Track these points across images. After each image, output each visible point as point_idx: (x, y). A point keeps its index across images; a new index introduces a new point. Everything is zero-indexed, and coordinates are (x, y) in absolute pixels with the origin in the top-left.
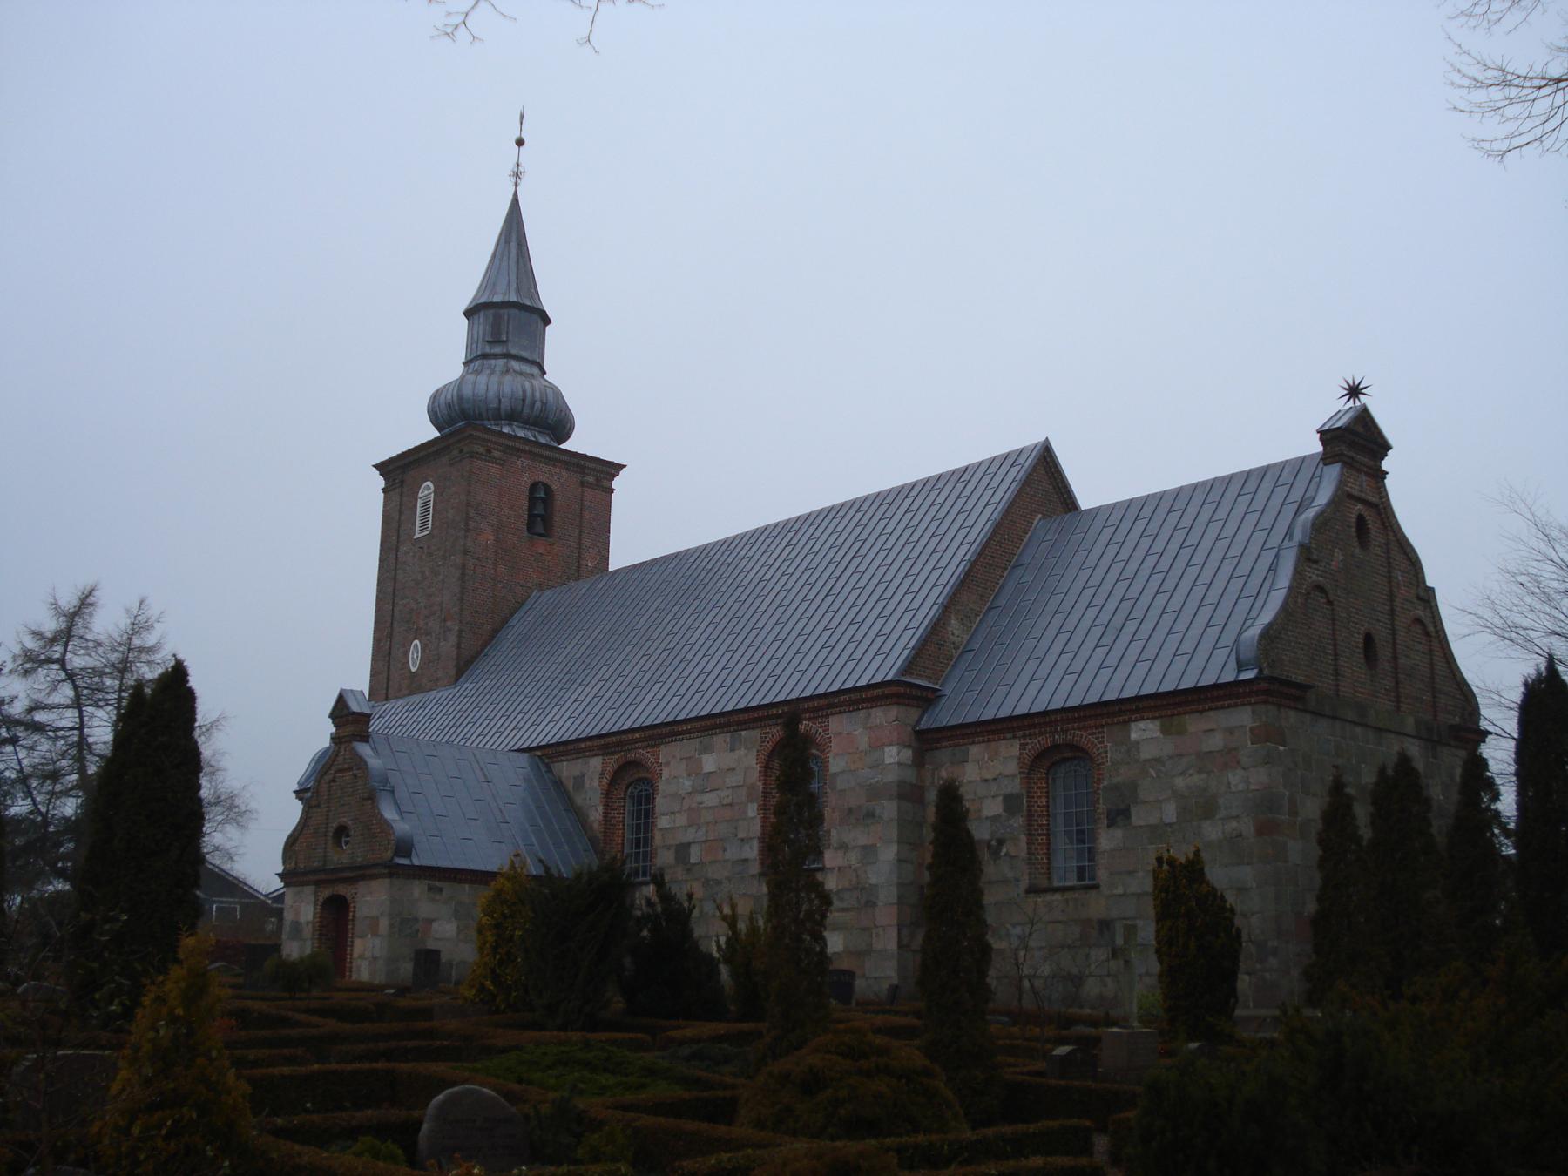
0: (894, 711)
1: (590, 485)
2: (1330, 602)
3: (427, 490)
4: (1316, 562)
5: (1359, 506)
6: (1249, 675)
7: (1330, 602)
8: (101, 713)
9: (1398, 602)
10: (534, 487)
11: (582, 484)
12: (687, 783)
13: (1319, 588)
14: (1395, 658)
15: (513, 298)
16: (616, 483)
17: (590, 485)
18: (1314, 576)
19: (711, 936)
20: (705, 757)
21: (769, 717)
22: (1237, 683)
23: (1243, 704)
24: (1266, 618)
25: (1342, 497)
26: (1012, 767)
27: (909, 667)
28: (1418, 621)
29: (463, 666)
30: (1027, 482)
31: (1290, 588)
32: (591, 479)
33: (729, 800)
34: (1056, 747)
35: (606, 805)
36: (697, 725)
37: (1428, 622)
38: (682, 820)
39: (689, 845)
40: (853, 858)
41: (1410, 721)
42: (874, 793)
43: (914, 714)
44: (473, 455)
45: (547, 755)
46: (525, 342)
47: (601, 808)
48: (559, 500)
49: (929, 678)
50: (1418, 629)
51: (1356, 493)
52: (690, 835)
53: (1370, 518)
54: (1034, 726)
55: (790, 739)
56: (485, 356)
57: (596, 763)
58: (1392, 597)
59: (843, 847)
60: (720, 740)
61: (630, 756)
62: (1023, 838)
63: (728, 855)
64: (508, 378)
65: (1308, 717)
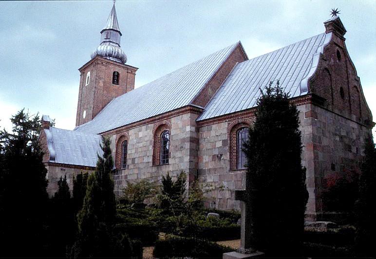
0: (189, 115)
1: (130, 73)
2: (330, 75)
3: (89, 74)
4: (325, 60)
5: (337, 47)
6: (306, 93)
7: (330, 75)
8: (310, 213)
9: (350, 79)
10: (114, 72)
11: (127, 72)
12: (135, 141)
13: (326, 69)
14: (349, 97)
15: (112, 28)
16: (136, 73)
17: (130, 73)
18: (325, 65)
19: (53, 175)
20: (140, 133)
21: (155, 120)
22: (300, 97)
23: (302, 104)
24: (310, 75)
25: (332, 43)
26: (225, 131)
27: (195, 100)
28: (355, 87)
29: (94, 116)
30: (233, 52)
31: (318, 67)
32: (130, 71)
33: (145, 145)
34: (239, 124)
35: (117, 148)
36: (138, 123)
37: (358, 87)
38: (133, 151)
39: (135, 158)
40: (177, 160)
41: (354, 116)
42: (183, 140)
43: (196, 116)
44: (98, 64)
45: (103, 135)
46: (114, 38)
47: (115, 149)
48: (121, 76)
49: (201, 106)
50: (355, 89)
51: (337, 43)
52: (136, 156)
53: (341, 51)
54: (231, 117)
55: (160, 124)
56: (104, 42)
57: (115, 136)
58: (348, 78)
59: (174, 157)
60: (144, 127)
61: (122, 133)
62: (228, 154)
63: (144, 161)
64: (109, 46)
65: (324, 111)
